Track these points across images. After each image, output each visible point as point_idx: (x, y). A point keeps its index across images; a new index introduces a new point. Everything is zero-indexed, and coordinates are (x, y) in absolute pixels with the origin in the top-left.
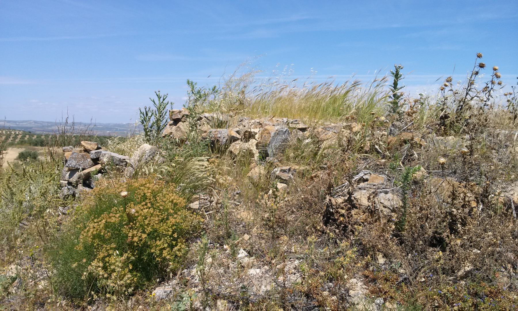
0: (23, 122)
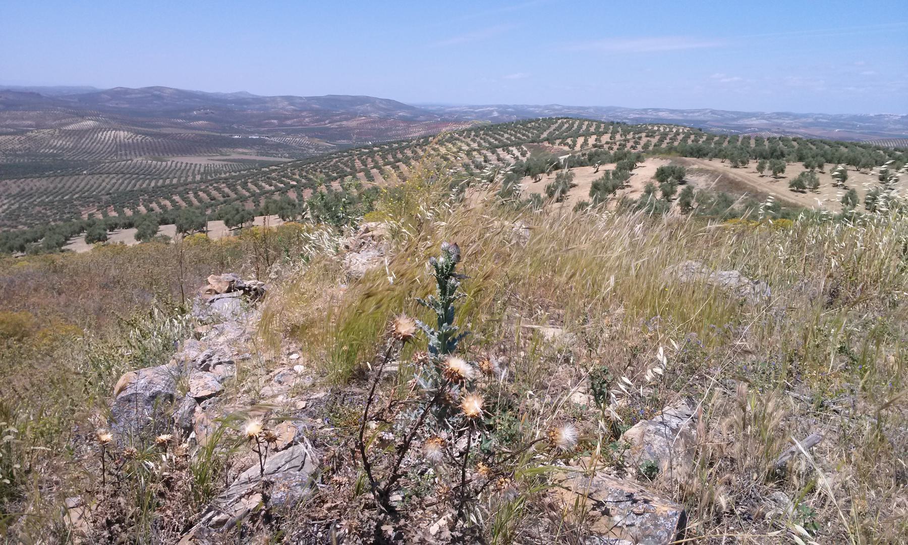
0: (693, 112)
